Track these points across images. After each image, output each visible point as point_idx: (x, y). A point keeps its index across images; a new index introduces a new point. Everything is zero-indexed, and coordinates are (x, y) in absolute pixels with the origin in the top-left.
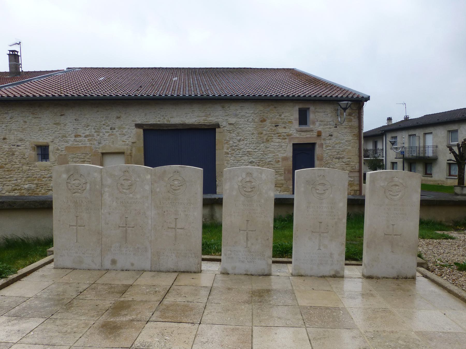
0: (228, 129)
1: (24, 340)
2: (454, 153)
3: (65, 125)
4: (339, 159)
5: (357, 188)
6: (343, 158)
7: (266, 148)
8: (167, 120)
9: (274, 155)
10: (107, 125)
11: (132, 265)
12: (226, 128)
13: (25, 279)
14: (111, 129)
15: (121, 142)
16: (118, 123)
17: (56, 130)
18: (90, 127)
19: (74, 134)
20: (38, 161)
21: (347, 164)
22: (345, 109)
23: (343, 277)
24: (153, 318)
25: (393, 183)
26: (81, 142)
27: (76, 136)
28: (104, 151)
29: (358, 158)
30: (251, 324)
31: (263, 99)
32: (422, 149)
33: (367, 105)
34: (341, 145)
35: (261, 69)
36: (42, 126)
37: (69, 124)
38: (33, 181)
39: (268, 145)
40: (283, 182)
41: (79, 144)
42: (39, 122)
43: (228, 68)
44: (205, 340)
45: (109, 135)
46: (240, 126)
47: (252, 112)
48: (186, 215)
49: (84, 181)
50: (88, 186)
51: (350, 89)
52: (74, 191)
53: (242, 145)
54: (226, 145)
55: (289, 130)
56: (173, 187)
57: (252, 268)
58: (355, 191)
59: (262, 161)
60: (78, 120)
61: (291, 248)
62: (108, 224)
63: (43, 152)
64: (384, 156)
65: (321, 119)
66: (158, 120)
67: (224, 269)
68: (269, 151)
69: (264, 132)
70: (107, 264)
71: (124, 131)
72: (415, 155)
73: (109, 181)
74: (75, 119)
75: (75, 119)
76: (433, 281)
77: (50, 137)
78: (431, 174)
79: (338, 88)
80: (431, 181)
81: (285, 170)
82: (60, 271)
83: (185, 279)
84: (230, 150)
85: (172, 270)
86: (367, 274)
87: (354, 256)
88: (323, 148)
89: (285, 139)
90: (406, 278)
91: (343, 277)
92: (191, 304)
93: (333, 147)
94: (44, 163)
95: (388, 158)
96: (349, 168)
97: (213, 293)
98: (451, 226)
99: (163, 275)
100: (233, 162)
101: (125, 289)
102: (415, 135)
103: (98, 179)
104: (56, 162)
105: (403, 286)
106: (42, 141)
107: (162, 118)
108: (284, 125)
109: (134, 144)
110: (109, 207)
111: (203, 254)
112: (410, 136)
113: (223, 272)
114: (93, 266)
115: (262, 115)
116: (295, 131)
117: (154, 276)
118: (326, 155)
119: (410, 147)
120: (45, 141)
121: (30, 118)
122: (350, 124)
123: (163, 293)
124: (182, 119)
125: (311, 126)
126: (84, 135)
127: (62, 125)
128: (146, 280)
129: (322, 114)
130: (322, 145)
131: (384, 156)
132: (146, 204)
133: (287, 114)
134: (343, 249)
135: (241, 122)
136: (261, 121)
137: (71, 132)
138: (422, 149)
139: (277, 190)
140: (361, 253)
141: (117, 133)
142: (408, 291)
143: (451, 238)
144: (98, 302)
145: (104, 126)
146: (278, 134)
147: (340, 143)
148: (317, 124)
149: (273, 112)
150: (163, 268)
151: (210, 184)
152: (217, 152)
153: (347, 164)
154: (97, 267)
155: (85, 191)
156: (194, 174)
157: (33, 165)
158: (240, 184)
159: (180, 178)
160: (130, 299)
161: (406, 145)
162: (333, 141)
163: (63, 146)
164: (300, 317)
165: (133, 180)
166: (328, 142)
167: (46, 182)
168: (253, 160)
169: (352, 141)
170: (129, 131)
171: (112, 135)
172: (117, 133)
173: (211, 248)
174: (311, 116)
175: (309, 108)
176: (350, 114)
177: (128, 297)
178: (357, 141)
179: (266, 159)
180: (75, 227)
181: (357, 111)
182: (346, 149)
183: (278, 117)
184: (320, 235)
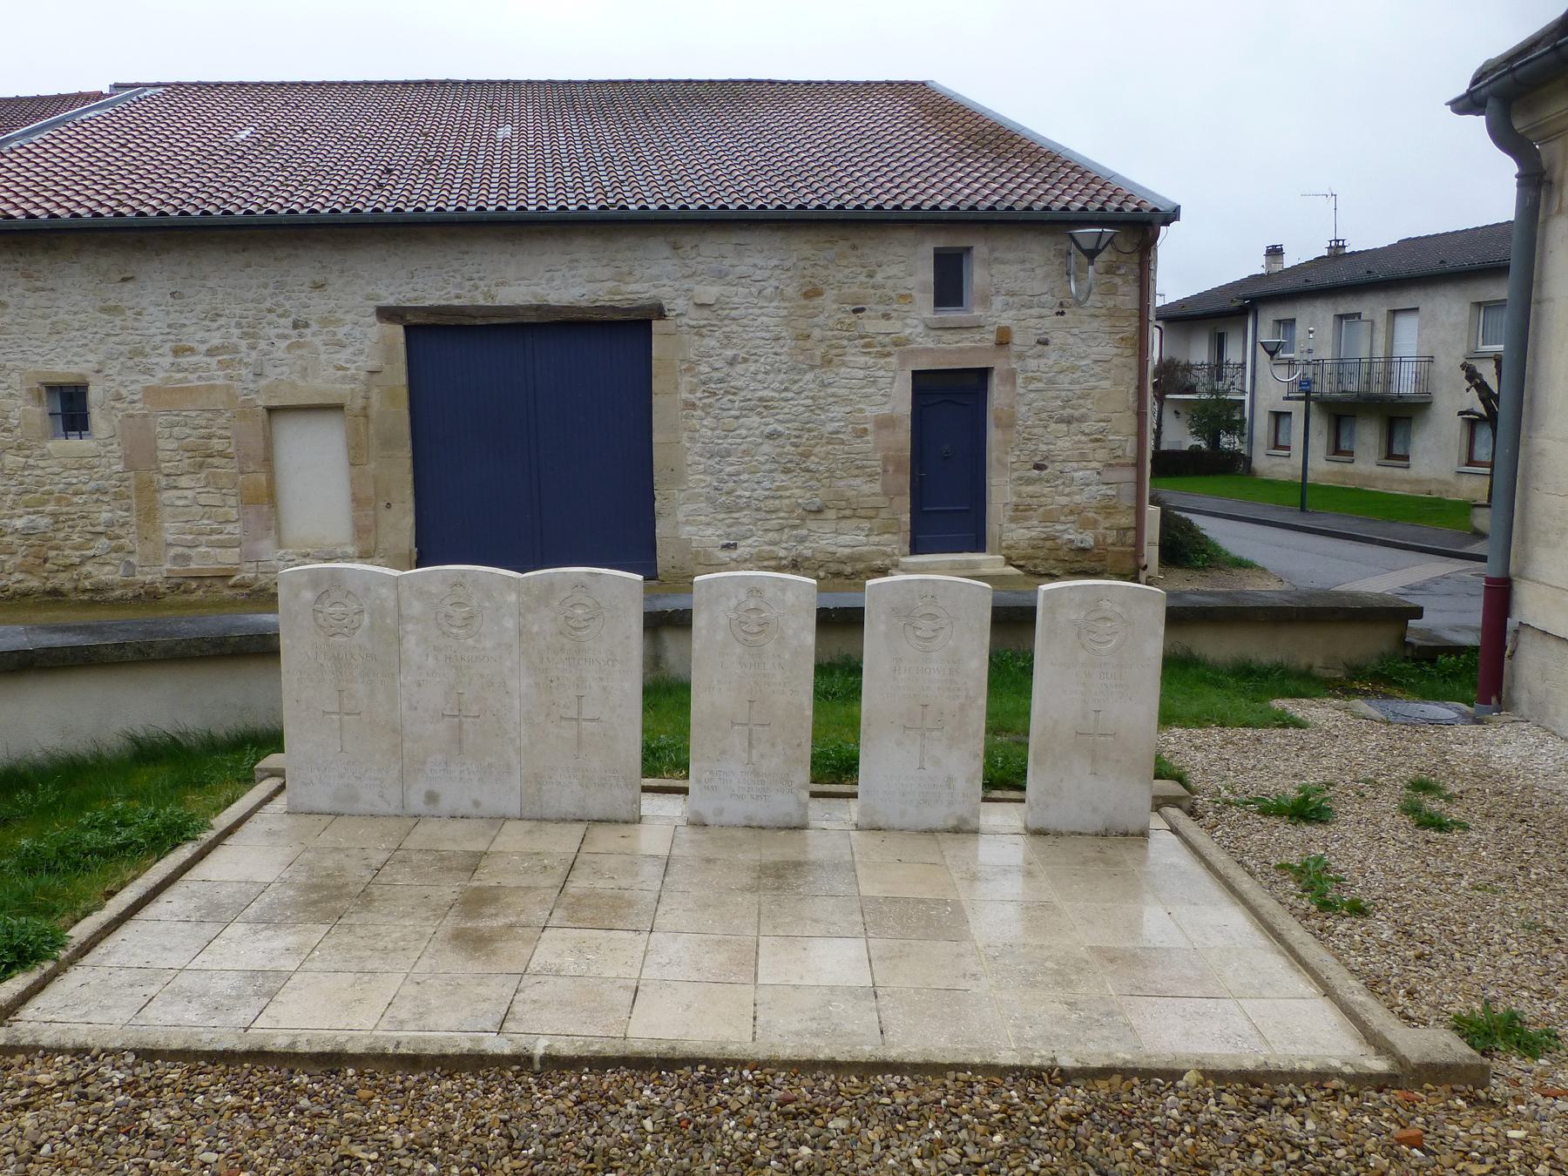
0: (693, 323)
1: (307, 965)
2: (1482, 387)
3: (140, 314)
4: (1069, 422)
5: (1127, 520)
6: (1082, 419)
7: (824, 385)
9: (848, 409)
10: (280, 311)
11: (476, 804)
12: (685, 320)
13: (230, 841)
14: (296, 326)
15: (331, 370)
16: (319, 305)
17: (108, 329)
18: (222, 321)
19: (170, 344)
20: (55, 436)
21: (1097, 440)
22: (1091, 254)
23: (976, 832)
24: (554, 922)
25: (1098, 615)
26: (195, 370)
27: (177, 352)
28: (275, 403)
29: (1134, 421)
30: (755, 933)
31: (811, 221)
32: (1379, 367)
33: (1168, 239)
34: (1079, 374)
35: (808, 83)
36: (61, 316)
37: (151, 309)
38: (43, 504)
39: (829, 377)
40: (881, 501)
41: (192, 377)
42: (49, 304)
43: (690, 82)
44: (664, 960)
45: (289, 347)
46: (734, 313)
47: (775, 262)
48: (605, 689)
51: (1115, 175)
53: (740, 377)
54: (687, 378)
55: (899, 324)
57: (762, 812)
58: (1123, 530)
59: (809, 430)
60: (181, 296)
61: (857, 759)
63: (70, 407)
64: (1248, 389)
65: (1008, 282)
66: (454, 292)
67: (697, 813)
68: (833, 395)
69: (817, 333)
70: (417, 803)
71: (341, 332)
72: (1353, 388)
73: (416, 608)
74: (172, 294)
75: (172, 294)
76: (1187, 842)
77: (91, 357)
78: (1406, 458)
79: (1073, 169)
80: (1407, 482)
81: (886, 459)
82: (304, 820)
83: (605, 839)
84: (699, 395)
86: (1033, 826)
87: (1004, 779)
88: (1014, 383)
89: (889, 354)
90: (1126, 834)
91: (976, 832)
92: (627, 894)
93: (1051, 382)
94: (75, 443)
95: (1260, 396)
96: (1102, 454)
97: (673, 869)
98: (1340, 680)
99: (551, 828)
100: (709, 433)
101: (473, 863)
102: (1359, 315)
103: (391, 604)
104: (115, 441)
105: (1110, 852)
106: (64, 369)
108: (882, 308)
109: (376, 377)
110: (419, 668)
111: (646, 774)
112: (1341, 317)
113: (692, 819)
114: (382, 808)
116: (920, 329)
117: (530, 832)
118: (1024, 409)
119: (1340, 362)
120: (74, 369)
121: (18, 290)
122: (1110, 304)
123: (562, 870)
124: (538, 290)
125: (977, 312)
126: (204, 347)
127: (129, 313)
128: (513, 839)
129: (1015, 268)
130: (1011, 376)
131: (1248, 389)
132: (508, 663)
133: (894, 270)
134: (977, 766)
135: (736, 299)
136: (807, 296)
137: (160, 337)
138: (1379, 367)
139: (858, 528)
140: (1023, 774)
141: (318, 341)
142: (1117, 864)
143: (1299, 724)
144: (426, 891)
145: (272, 317)
146: (862, 337)
147: (1073, 369)
148: (998, 302)
149: (844, 262)
151: (665, 623)
152: (657, 401)
153: (1097, 440)
154: (391, 810)
155: (358, 632)
156: (620, 587)
157: (37, 452)
158: (734, 616)
159: (588, 601)
160: (493, 884)
161: (1326, 353)
162: (1051, 362)
163: (138, 387)
164: (860, 918)
166: (1032, 364)
167: (86, 508)
168: (780, 428)
169: (1117, 361)
170: (357, 332)
171: (299, 345)
172: (318, 341)
173: (664, 760)
174: (977, 276)
175: (969, 249)
176: (1110, 270)
177: (486, 878)
178: (1134, 362)
179: (823, 423)
181: (1136, 258)
182: (1094, 388)
183: (862, 278)
184: (923, 735)
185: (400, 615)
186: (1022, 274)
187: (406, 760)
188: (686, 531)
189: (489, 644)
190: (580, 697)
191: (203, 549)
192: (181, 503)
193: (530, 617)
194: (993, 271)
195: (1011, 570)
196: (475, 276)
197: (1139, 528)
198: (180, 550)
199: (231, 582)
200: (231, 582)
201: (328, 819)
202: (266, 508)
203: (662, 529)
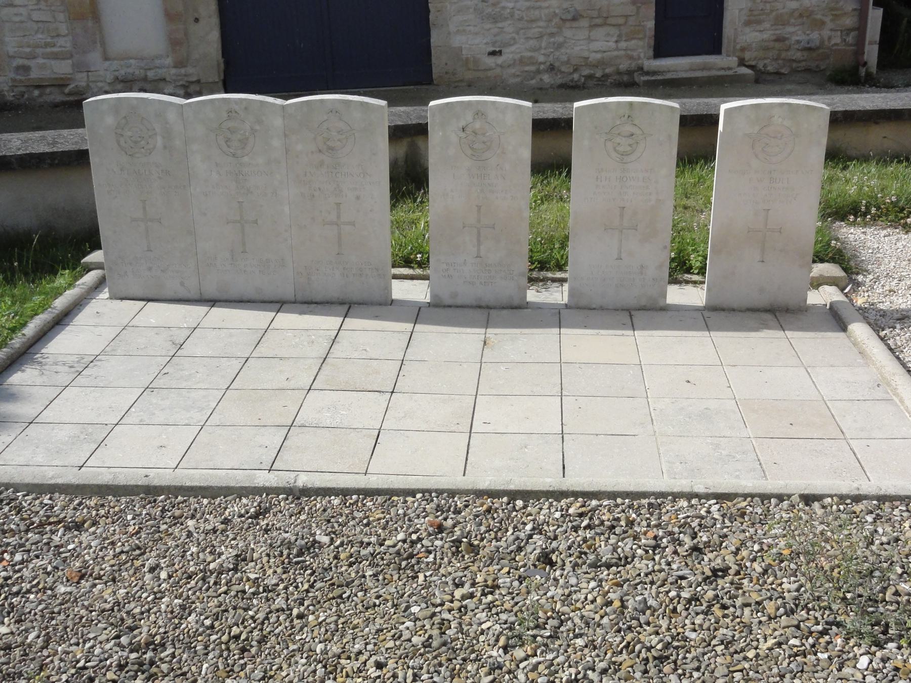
139: (608, 35)
188: (457, 41)
190: (338, 204)
191: (41, 61)
192: (17, 19)
195: (744, 70)
197: (861, 29)
198: (20, 62)
199: (67, 90)
200: (67, 90)
202: (90, 24)
203: (436, 38)
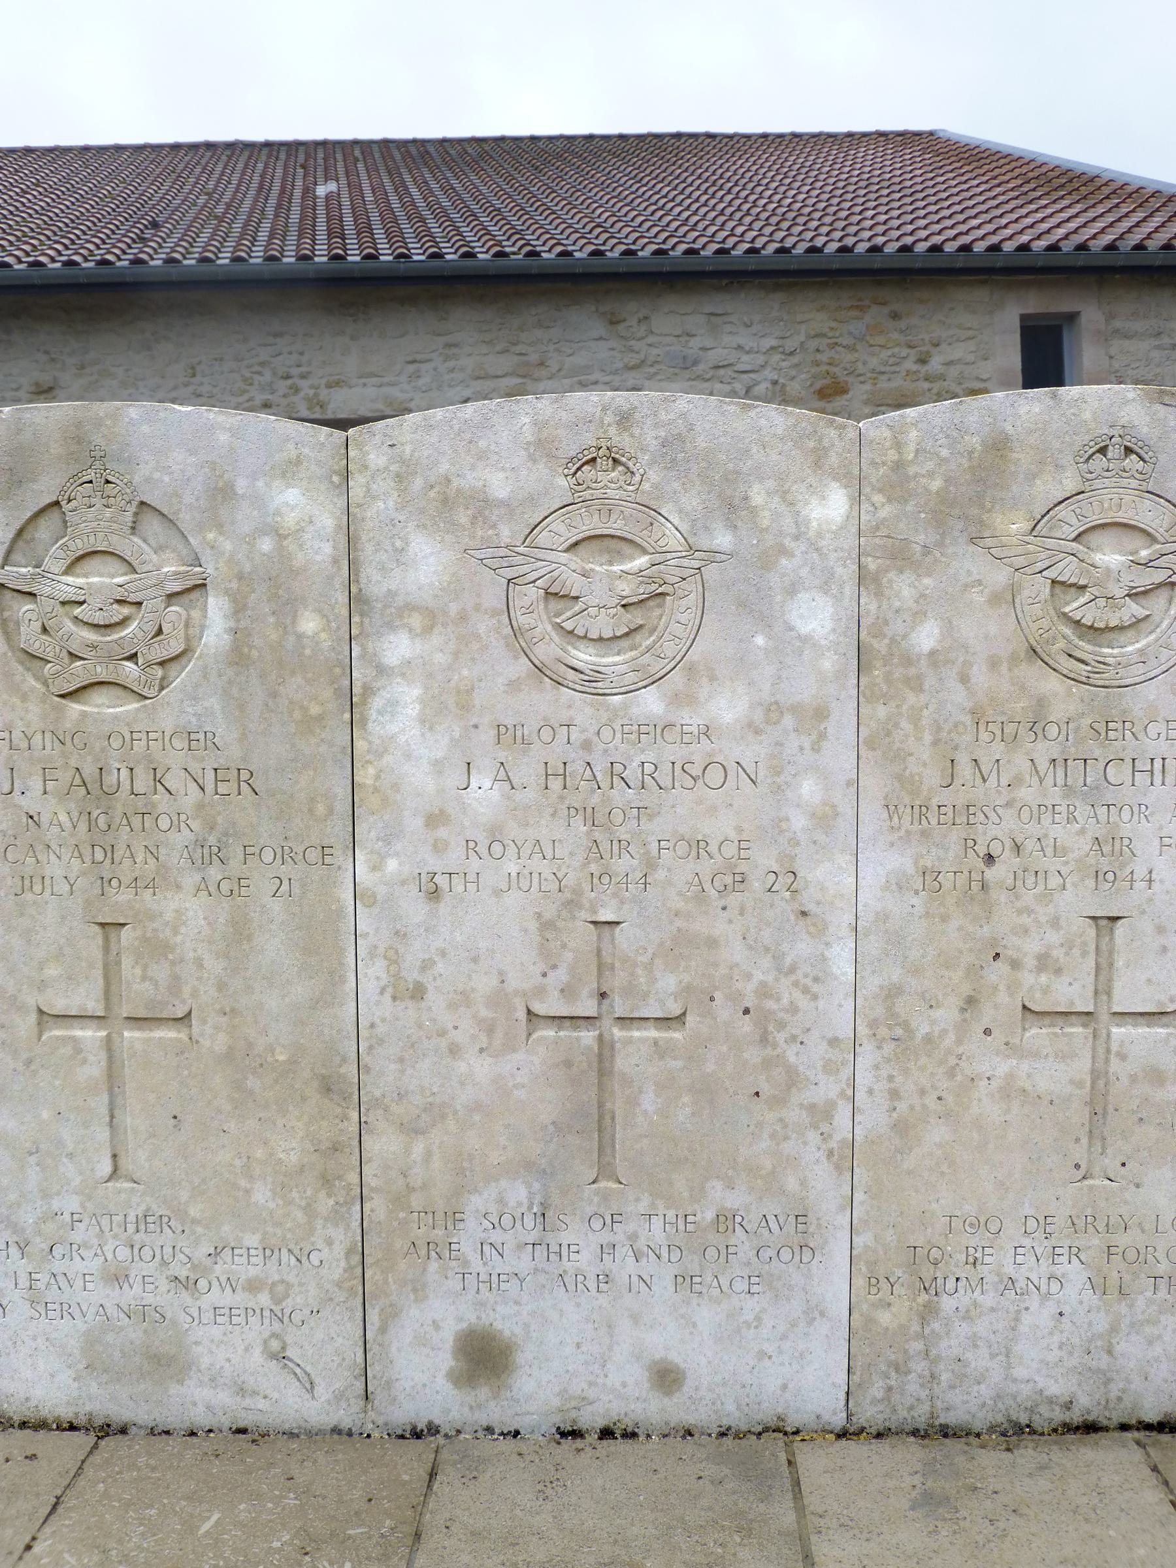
8: (308, 400)
11: (666, 1377)
47: (770, 342)
49: (171, 568)
50: (215, 621)
52: (79, 673)
56: (1074, 606)
62: (418, 993)
70: (423, 1381)
73: (424, 563)
85: (1059, 1416)
103: (320, 550)
107: (282, 386)
110: (435, 819)
114: (284, 1401)
115: (823, 357)
129: (1144, 345)
132: (809, 789)
133: (959, 352)
149: (881, 340)
150: (966, 1404)
154: (318, 1408)
155: (182, 678)
159: (1150, 515)
165: (673, 541)
175: (1072, 317)
180: (89, 1034)
183: (909, 365)
185: (356, 600)
186: (1155, 354)
187: (377, 1207)
189: (727, 707)
193: (903, 588)
194: (1113, 351)
196: (295, 371)
201: (83, 1441)
